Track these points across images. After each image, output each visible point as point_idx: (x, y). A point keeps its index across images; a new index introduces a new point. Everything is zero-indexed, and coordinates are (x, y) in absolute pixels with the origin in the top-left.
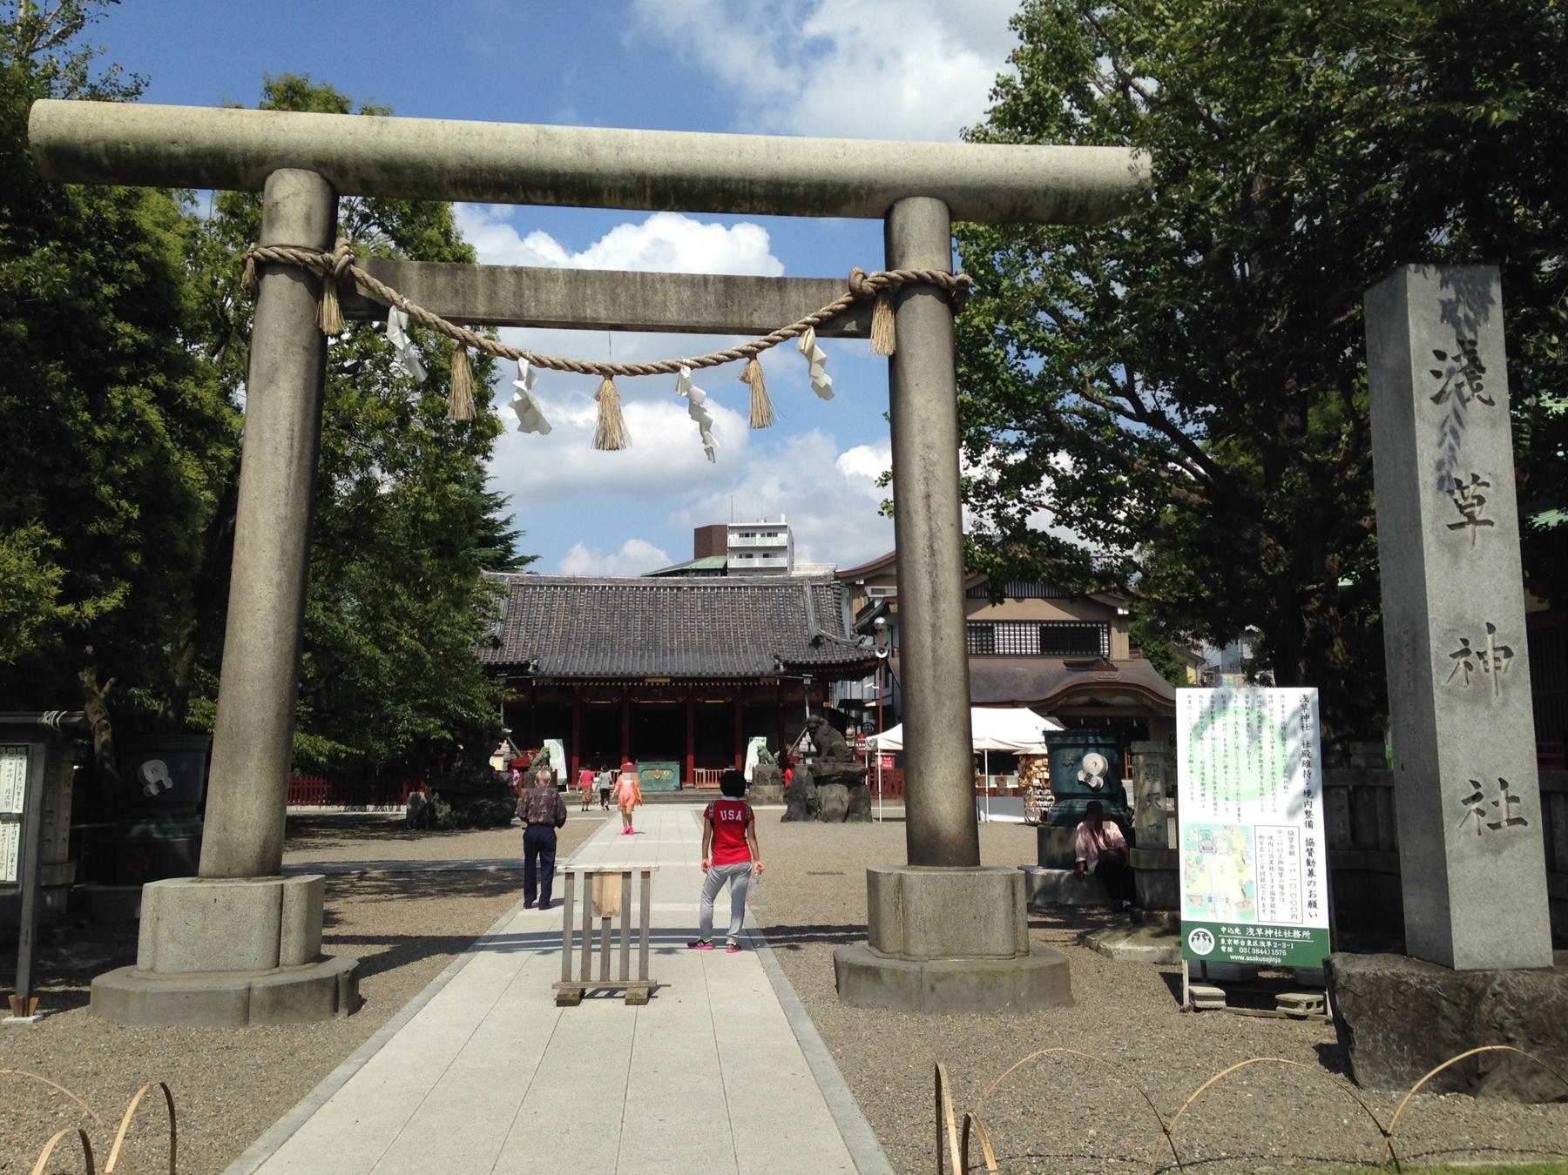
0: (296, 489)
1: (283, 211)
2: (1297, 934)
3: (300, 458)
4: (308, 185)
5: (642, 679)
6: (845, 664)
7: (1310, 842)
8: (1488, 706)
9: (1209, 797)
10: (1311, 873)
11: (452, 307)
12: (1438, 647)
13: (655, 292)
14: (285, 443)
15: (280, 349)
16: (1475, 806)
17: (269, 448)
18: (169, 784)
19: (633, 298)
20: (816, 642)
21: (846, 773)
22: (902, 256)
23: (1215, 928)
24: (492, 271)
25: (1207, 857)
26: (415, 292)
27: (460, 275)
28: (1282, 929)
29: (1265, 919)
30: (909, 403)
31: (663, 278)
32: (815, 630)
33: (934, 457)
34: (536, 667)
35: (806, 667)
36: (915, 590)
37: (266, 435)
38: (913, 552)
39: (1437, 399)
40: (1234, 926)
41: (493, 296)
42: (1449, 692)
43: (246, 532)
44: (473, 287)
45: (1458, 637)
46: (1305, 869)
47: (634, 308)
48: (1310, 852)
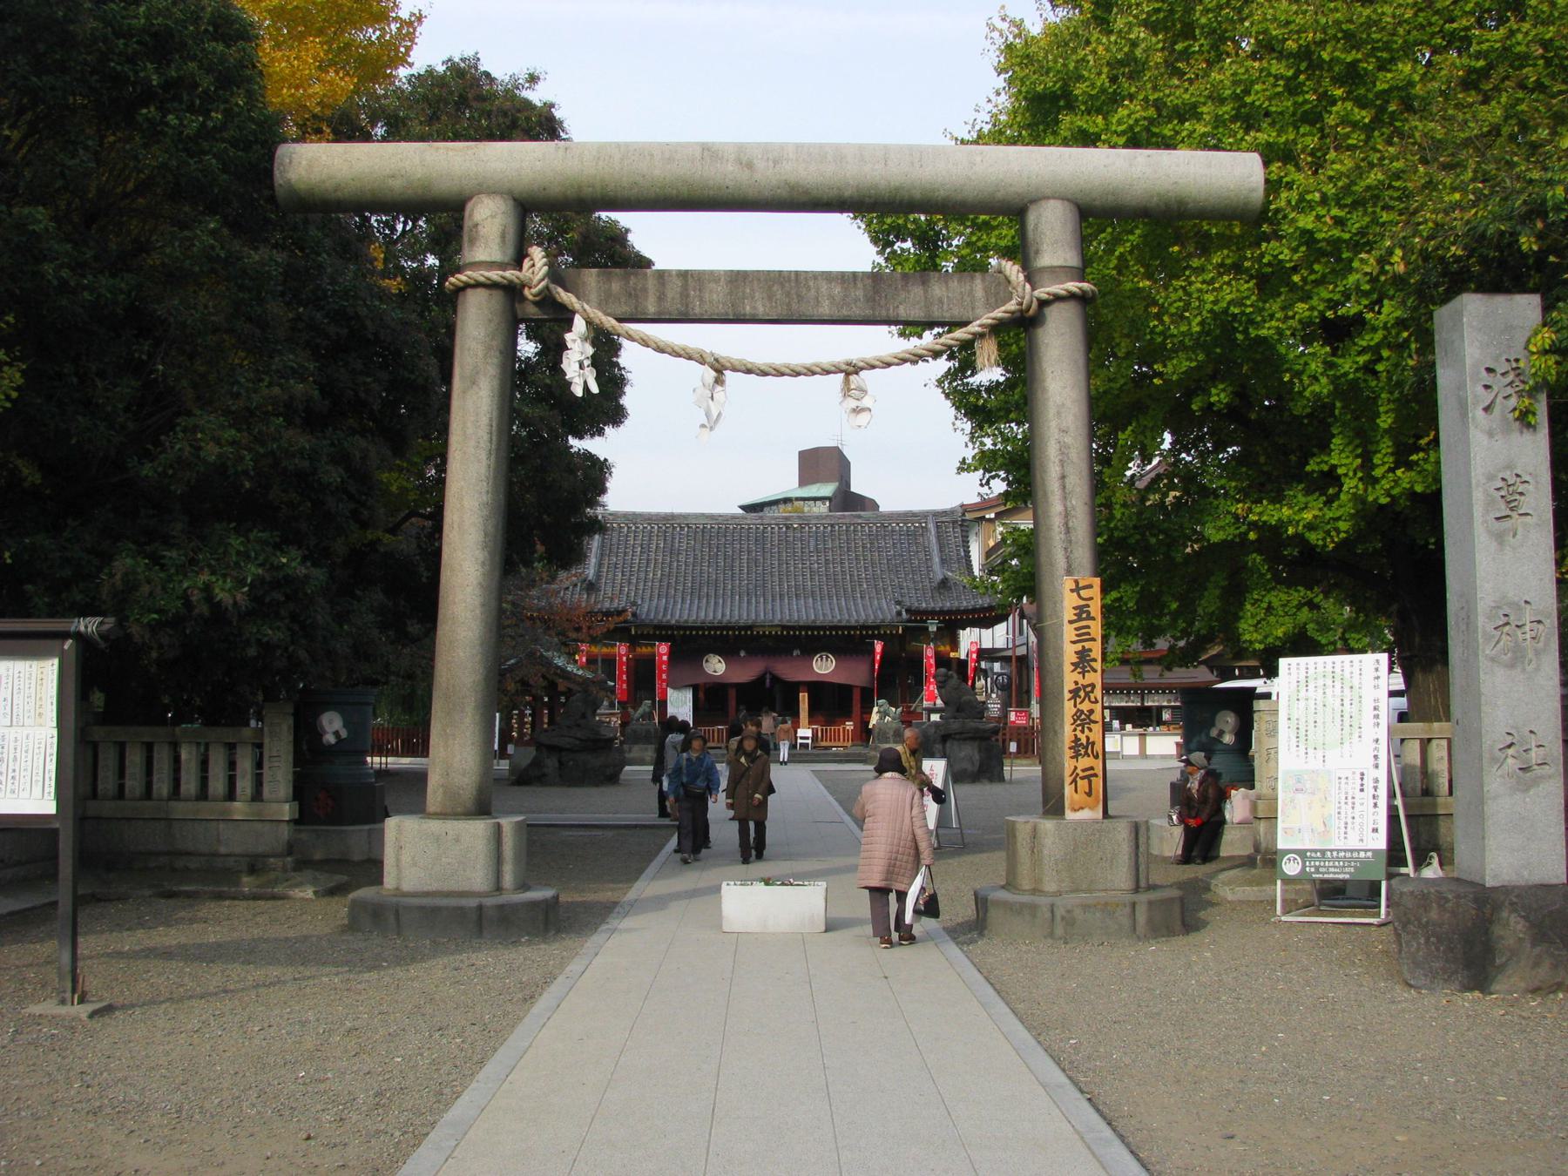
0: (495, 478)
1: (483, 231)
2: (1362, 854)
3: (498, 449)
4: (503, 208)
5: (750, 628)
6: (974, 610)
7: (1376, 781)
8: (1524, 670)
9: (1302, 747)
10: (1375, 805)
11: (624, 309)
12: (1483, 623)
13: (809, 289)
14: (486, 437)
15: (480, 354)
16: (1511, 751)
17: (472, 443)
18: (344, 734)
19: (788, 294)
20: (944, 584)
21: (977, 730)
22: (1037, 252)
23: (1302, 853)
24: (661, 274)
25: (1300, 796)
26: (593, 296)
27: (633, 280)
28: (1352, 851)
29: (1340, 845)
30: (1044, 390)
31: (816, 276)
32: (938, 573)
33: (1068, 440)
34: (634, 615)
35: (932, 613)
36: (1052, 565)
37: (470, 431)
38: (1049, 529)
39: (1487, 409)
40: (1316, 851)
41: (661, 298)
42: (1493, 659)
43: (455, 518)
44: (645, 290)
45: (1501, 612)
46: (1372, 802)
47: (789, 304)
48: (1375, 788)
